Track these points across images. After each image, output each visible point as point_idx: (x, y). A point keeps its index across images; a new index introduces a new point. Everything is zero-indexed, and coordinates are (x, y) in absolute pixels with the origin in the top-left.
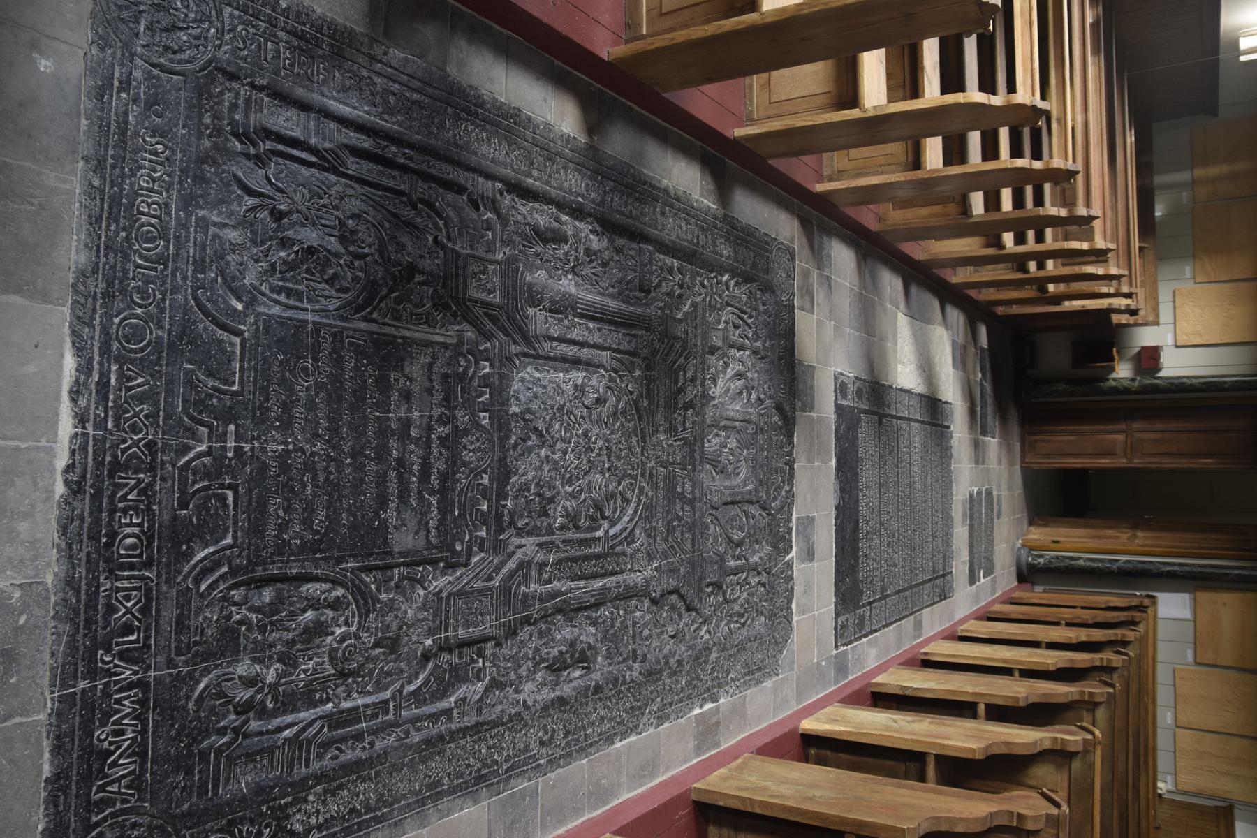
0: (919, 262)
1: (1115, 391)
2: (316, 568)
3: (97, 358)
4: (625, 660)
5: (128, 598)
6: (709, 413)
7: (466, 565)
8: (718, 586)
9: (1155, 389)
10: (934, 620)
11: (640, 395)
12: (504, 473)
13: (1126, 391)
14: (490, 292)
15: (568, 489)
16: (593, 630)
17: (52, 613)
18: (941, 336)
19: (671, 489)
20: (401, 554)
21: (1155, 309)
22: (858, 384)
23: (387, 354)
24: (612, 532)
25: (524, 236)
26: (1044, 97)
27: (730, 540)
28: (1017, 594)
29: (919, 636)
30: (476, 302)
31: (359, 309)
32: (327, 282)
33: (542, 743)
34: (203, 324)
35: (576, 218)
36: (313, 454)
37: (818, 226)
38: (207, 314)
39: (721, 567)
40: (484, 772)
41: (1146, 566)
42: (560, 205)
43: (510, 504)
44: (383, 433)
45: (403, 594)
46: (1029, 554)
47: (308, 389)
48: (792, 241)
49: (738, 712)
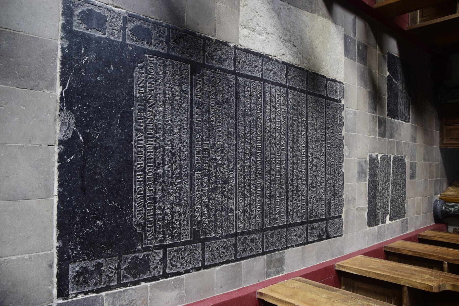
28: (429, 234)
46: (444, 203)
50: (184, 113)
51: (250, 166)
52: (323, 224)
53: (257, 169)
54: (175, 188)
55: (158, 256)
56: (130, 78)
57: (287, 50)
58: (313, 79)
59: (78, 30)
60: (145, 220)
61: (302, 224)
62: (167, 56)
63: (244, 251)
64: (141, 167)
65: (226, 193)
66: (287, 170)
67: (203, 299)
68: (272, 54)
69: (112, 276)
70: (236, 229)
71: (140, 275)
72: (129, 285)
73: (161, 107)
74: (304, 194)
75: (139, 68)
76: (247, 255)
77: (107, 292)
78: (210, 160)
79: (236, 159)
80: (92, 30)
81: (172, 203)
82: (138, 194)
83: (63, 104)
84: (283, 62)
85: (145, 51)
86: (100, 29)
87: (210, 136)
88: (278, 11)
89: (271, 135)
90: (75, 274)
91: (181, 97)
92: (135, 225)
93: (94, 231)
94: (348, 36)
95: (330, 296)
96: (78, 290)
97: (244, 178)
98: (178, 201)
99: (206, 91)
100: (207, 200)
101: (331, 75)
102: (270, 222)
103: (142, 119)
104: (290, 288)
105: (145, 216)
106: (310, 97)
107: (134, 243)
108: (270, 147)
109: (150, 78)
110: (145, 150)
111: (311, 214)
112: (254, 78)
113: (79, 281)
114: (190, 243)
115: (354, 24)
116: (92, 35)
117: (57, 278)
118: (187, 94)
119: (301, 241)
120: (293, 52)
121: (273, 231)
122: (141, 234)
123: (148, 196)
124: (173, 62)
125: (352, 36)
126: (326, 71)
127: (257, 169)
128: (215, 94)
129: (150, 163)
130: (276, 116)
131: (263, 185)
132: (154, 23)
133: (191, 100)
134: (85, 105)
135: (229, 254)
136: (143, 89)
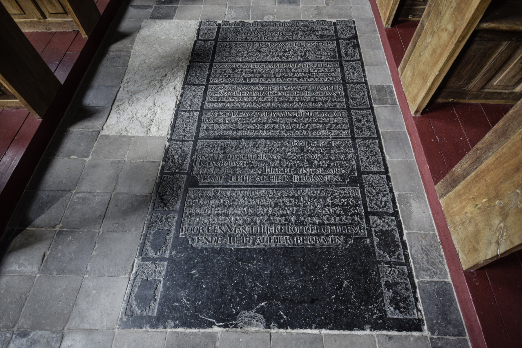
50: (237, 194)
51: (286, 123)
52: (342, 43)
53: (288, 117)
54: (309, 203)
55: (376, 221)
56: (203, 253)
57: (170, 84)
58: (198, 55)
59: (156, 310)
60: (341, 234)
61: (342, 67)
62: (181, 212)
63: (369, 129)
64: (289, 239)
65: (313, 149)
66: (289, 84)
67: (419, 173)
68: (175, 100)
69: (398, 271)
70: (347, 138)
71: (396, 241)
72: (406, 253)
73: (231, 218)
74: (312, 65)
75: (193, 243)
76: (373, 126)
77: (415, 277)
78: (281, 166)
79: (279, 138)
80: (156, 295)
81: (324, 206)
82: (316, 242)
83: (230, 324)
84: (183, 88)
85: (177, 237)
86: (155, 286)
87: (257, 167)
88: (130, 93)
89: (255, 101)
90: (397, 311)
91: (221, 198)
92: (346, 246)
93: (353, 290)
94: (152, 15)
95: (429, 33)
96: (414, 309)
97: (298, 129)
98: (321, 200)
99: (214, 170)
100: (319, 169)
101: (193, 35)
102: (341, 102)
103: (243, 238)
104: (412, 79)
105: (337, 235)
106: (217, 59)
107: (364, 246)
108: (267, 102)
109: (203, 231)
110: (273, 235)
111: (332, 57)
112: (200, 119)
113: (404, 308)
114: (362, 187)
115: (139, 7)
116: (161, 295)
117: (402, 331)
118: (217, 191)
119: (359, 67)
120: (172, 78)
121: (350, 98)
122: (355, 239)
123: (317, 232)
124: (187, 207)
125: (151, 10)
126: (189, 40)
127: (288, 117)
128: (216, 161)
129: (285, 229)
130: (236, 96)
131: (304, 109)
132: (149, 228)
133: (224, 186)
134: (231, 300)
135: (372, 145)
136: (213, 238)
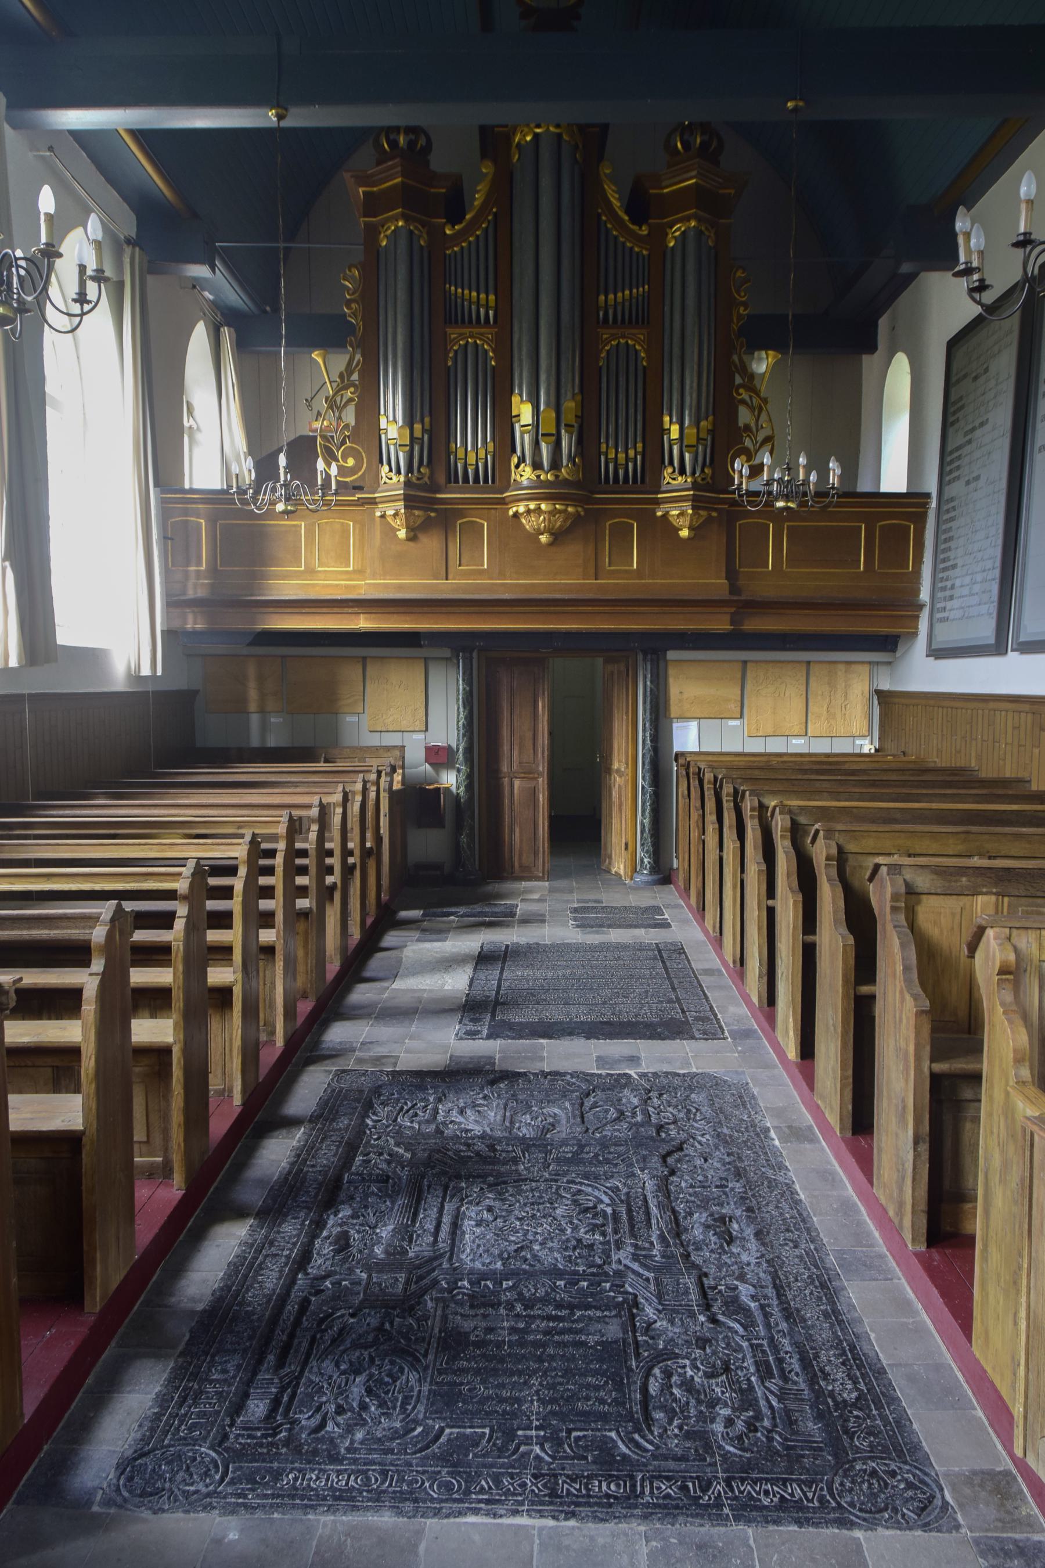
0: (342, 966)
1: (469, 787)
2: (636, 1383)
3: (466, 1505)
4: (725, 1193)
5: (659, 1488)
6: (499, 1134)
7: (636, 1296)
8: (660, 1128)
9: (469, 750)
10: (704, 958)
11: (484, 1182)
12: (555, 1273)
13: (470, 777)
14: (397, 1280)
15: (569, 1231)
16: (696, 1216)
17: (669, 1526)
18: (414, 951)
19: (568, 1161)
20: (625, 1332)
21: (388, 749)
22: (466, 1021)
23: (454, 1343)
24: (607, 1200)
25: (344, 1260)
26: (242, 836)
27: (618, 1119)
28: (681, 883)
29: (720, 971)
30: (406, 1289)
31: (418, 1360)
32: (395, 1381)
33: (796, 1247)
34: (435, 1448)
35: (325, 1226)
36: (541, 1384)
37: (311, 1051)
38: (427, 1447)
39: (642, 1126)
40: (817, 1283)
41: (647, 761)
42: (313, 1236)
43: (581, 1269)
44: (522, 1344)
45: (659, 1336)
47: (485, 1388)
48: (330, 1072)
49: (778, 1113)
